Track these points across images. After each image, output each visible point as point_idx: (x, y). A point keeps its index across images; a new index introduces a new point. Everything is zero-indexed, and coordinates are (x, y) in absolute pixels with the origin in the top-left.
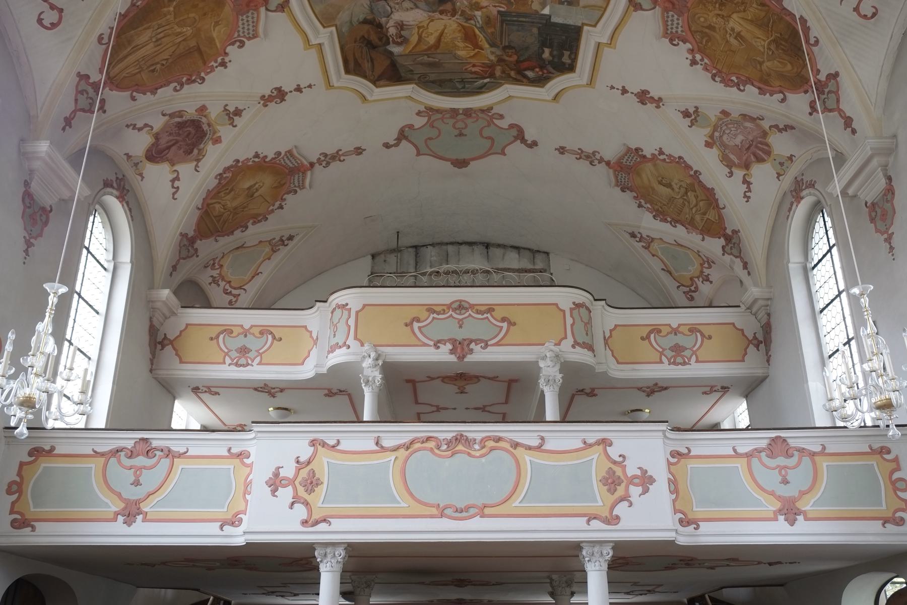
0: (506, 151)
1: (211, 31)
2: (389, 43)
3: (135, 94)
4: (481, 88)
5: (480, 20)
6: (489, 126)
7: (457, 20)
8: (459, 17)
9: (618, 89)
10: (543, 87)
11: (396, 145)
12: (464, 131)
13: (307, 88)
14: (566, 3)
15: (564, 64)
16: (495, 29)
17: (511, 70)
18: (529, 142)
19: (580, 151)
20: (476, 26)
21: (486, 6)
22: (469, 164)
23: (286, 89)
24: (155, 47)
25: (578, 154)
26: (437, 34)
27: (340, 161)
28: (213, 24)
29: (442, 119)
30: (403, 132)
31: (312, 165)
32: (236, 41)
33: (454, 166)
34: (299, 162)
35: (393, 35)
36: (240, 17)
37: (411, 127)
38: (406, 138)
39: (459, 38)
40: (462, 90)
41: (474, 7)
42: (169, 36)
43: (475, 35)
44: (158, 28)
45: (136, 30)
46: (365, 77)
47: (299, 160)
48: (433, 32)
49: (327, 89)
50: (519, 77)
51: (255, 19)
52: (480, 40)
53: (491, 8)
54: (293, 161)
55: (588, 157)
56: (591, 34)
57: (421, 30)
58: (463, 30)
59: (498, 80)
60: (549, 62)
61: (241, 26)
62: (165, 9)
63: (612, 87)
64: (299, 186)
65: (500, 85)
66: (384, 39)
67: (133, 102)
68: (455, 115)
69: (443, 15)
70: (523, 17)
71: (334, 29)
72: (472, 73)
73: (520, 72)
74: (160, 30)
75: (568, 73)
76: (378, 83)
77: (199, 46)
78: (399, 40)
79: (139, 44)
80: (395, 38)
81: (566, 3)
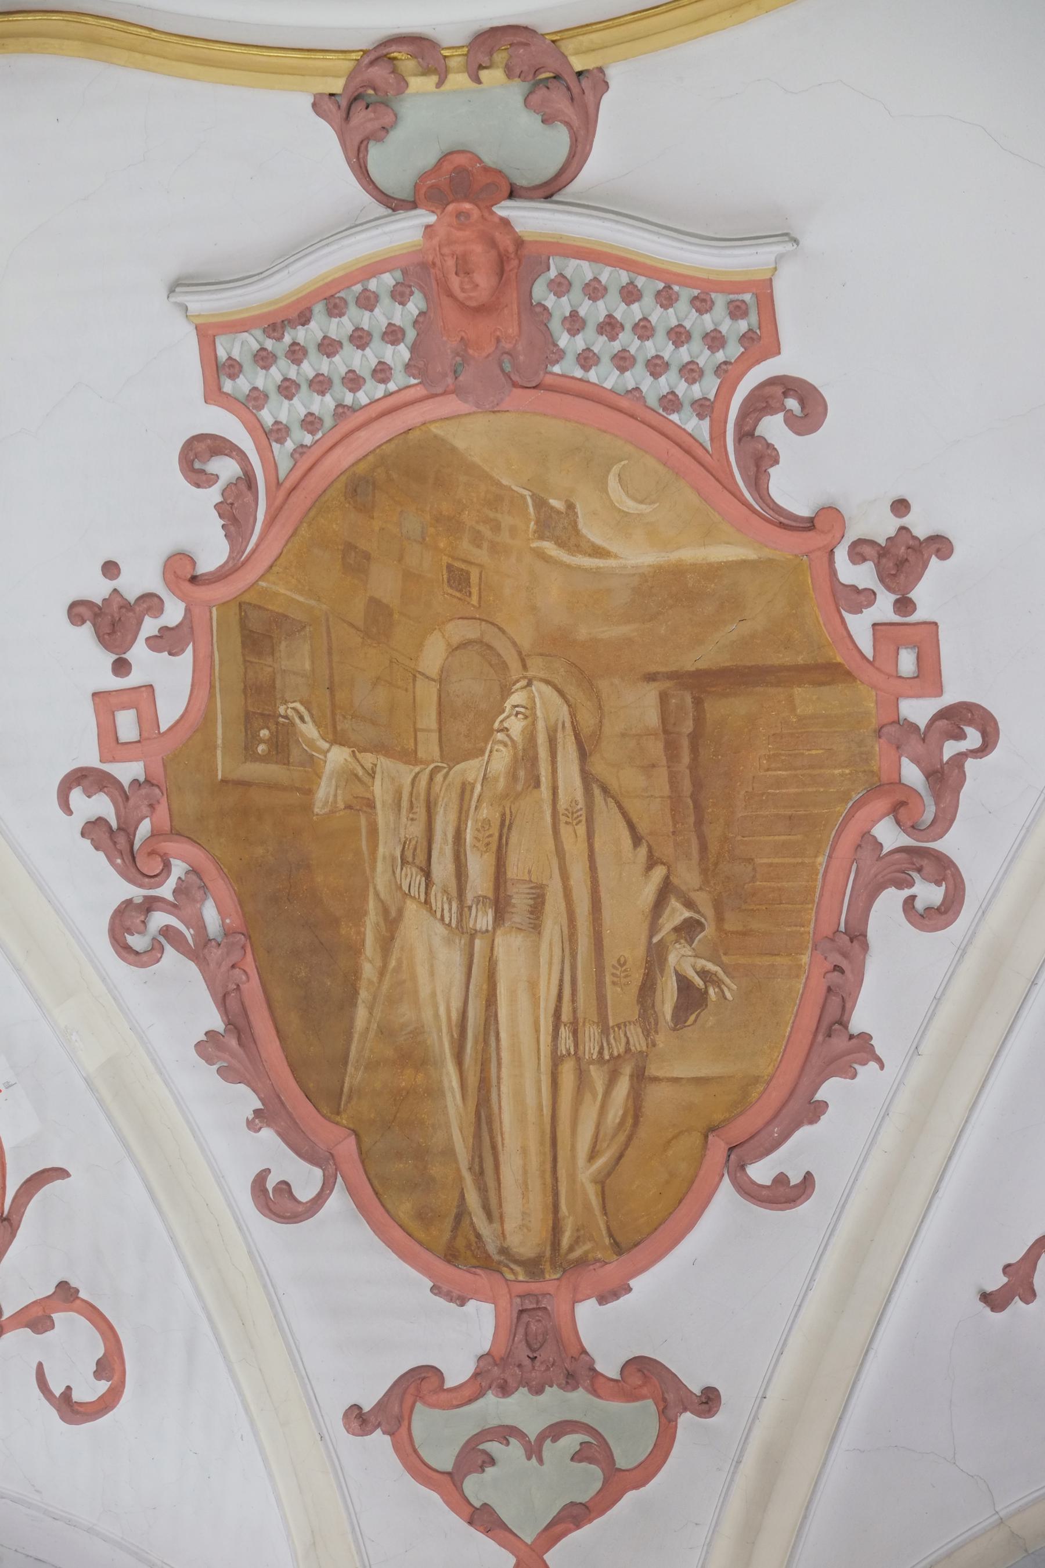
1: (597, 572)
3: (761, 1172)
24: (536, 927)
28: (549, 547)
32: (746, 434)
36: (567, 367)
42: (505, 825)
44: (427, 874)
45: (364, 995)
51: (606, 275)
61: (637, 377)
62: (324, 792)
67: (805, 1208)
74: (443, 869)
77: (675, 676)
79: (456, 1004)
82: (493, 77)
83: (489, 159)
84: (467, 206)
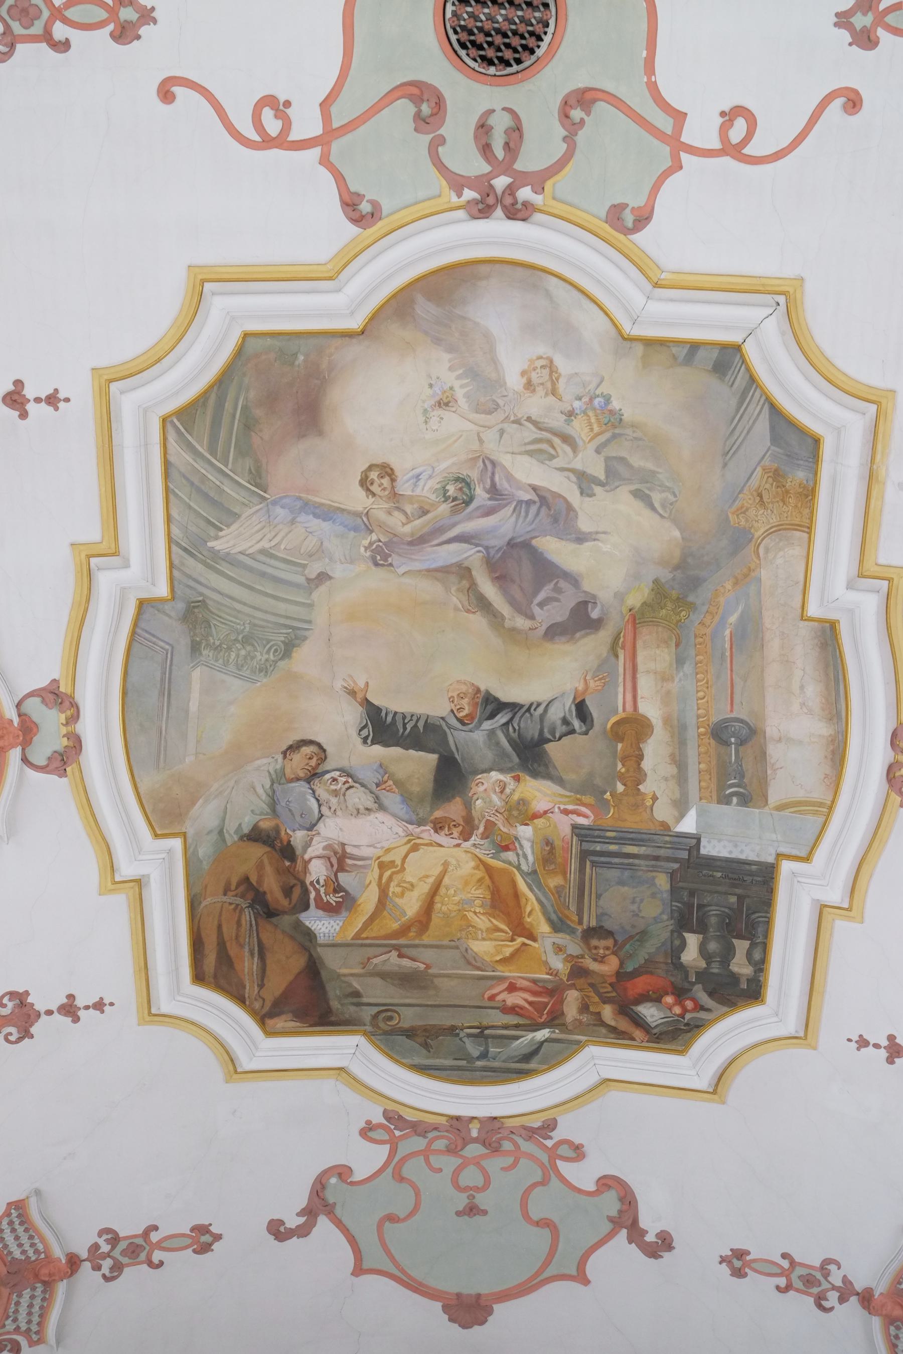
0: (591, 1268)
2: (306, 907)
4: (527, 1057)
5: (529, 852)
6: (544, 1182)
7: (473, 849)
8: (479, 841)
9: (877, 1046)
10: (681, 1052)
11: (303, 1231)
12: (482, 1200)
13: (91, 1011)
14: (735, 800)
15: (735, 978)
16: (564, 874)
17: (604, 1003)
18: (650, 1238)
19: (785, 1264)
20: (518, 868)
21: (546, 812)
22: (490, 1311)
23: (39, 1001)
25: (783, 1273)
26: (424, 888)
27: (151, 1264)
29: (426, 1153)
30: (323, 1187)
31: (74, 1262)
33: (450, 1320)
34: (40, 1247)
35: (318, 882)
37: (343, 1172)
38: (329, 1210)
39: (478, 902)
40: (479, 1063)
41: (515, 813)
43: (516, 895)
46: (240, 999)
47: (43, 1240)
48: (414, 881)
49: (142, 1022)
50: (623, 1024)
52: (528, 909)
53: (557, 817)
54: (24, 1240)
55: (809, 1281)
56: (799, 879)
57: (387, 874)
58: (487, 881)
59: (571, 1032)
60: (698, 974)
63: (863, 1043)
64: (29, 1330)
65: (579, 1046)
66: (297, 892)
68: (460, 1142)
69: (443, 833)
70: (634, 842)
71: (176, 844)
72: (508, 1010)
73: (625, 1009)
75: (747, 1006)
76: (270, 1022)
78: (333, 899)
80: (322, 890)
81: (735, 800)
82: (65, 742)
83: (35, 739)
84: (21, 738)
